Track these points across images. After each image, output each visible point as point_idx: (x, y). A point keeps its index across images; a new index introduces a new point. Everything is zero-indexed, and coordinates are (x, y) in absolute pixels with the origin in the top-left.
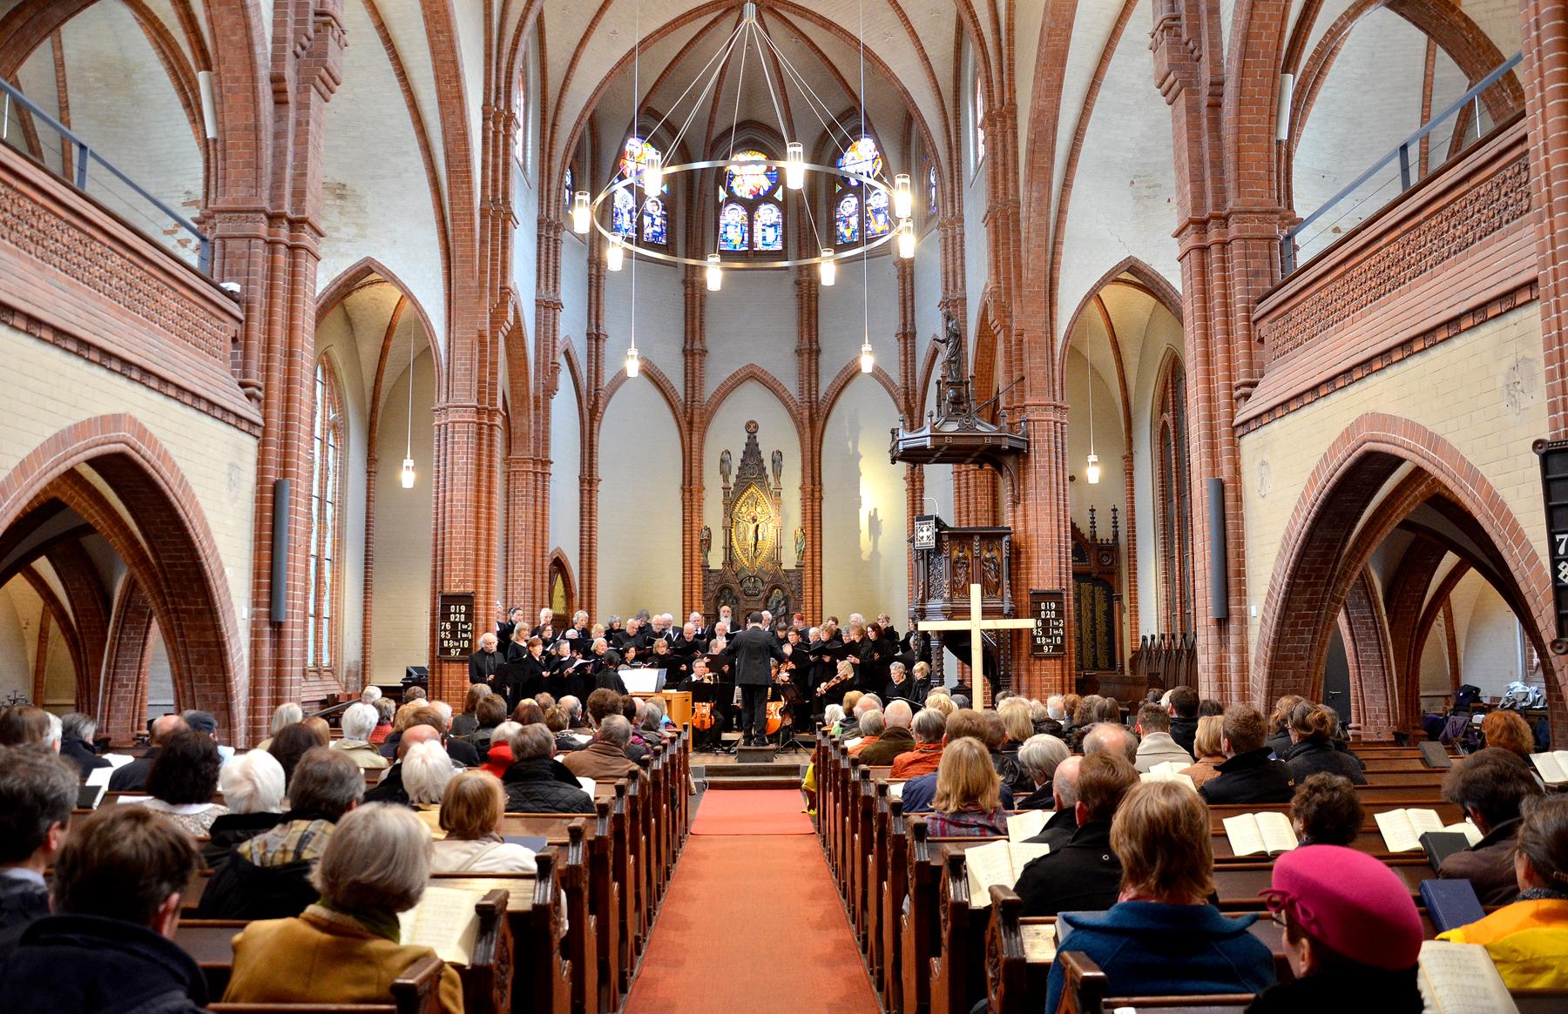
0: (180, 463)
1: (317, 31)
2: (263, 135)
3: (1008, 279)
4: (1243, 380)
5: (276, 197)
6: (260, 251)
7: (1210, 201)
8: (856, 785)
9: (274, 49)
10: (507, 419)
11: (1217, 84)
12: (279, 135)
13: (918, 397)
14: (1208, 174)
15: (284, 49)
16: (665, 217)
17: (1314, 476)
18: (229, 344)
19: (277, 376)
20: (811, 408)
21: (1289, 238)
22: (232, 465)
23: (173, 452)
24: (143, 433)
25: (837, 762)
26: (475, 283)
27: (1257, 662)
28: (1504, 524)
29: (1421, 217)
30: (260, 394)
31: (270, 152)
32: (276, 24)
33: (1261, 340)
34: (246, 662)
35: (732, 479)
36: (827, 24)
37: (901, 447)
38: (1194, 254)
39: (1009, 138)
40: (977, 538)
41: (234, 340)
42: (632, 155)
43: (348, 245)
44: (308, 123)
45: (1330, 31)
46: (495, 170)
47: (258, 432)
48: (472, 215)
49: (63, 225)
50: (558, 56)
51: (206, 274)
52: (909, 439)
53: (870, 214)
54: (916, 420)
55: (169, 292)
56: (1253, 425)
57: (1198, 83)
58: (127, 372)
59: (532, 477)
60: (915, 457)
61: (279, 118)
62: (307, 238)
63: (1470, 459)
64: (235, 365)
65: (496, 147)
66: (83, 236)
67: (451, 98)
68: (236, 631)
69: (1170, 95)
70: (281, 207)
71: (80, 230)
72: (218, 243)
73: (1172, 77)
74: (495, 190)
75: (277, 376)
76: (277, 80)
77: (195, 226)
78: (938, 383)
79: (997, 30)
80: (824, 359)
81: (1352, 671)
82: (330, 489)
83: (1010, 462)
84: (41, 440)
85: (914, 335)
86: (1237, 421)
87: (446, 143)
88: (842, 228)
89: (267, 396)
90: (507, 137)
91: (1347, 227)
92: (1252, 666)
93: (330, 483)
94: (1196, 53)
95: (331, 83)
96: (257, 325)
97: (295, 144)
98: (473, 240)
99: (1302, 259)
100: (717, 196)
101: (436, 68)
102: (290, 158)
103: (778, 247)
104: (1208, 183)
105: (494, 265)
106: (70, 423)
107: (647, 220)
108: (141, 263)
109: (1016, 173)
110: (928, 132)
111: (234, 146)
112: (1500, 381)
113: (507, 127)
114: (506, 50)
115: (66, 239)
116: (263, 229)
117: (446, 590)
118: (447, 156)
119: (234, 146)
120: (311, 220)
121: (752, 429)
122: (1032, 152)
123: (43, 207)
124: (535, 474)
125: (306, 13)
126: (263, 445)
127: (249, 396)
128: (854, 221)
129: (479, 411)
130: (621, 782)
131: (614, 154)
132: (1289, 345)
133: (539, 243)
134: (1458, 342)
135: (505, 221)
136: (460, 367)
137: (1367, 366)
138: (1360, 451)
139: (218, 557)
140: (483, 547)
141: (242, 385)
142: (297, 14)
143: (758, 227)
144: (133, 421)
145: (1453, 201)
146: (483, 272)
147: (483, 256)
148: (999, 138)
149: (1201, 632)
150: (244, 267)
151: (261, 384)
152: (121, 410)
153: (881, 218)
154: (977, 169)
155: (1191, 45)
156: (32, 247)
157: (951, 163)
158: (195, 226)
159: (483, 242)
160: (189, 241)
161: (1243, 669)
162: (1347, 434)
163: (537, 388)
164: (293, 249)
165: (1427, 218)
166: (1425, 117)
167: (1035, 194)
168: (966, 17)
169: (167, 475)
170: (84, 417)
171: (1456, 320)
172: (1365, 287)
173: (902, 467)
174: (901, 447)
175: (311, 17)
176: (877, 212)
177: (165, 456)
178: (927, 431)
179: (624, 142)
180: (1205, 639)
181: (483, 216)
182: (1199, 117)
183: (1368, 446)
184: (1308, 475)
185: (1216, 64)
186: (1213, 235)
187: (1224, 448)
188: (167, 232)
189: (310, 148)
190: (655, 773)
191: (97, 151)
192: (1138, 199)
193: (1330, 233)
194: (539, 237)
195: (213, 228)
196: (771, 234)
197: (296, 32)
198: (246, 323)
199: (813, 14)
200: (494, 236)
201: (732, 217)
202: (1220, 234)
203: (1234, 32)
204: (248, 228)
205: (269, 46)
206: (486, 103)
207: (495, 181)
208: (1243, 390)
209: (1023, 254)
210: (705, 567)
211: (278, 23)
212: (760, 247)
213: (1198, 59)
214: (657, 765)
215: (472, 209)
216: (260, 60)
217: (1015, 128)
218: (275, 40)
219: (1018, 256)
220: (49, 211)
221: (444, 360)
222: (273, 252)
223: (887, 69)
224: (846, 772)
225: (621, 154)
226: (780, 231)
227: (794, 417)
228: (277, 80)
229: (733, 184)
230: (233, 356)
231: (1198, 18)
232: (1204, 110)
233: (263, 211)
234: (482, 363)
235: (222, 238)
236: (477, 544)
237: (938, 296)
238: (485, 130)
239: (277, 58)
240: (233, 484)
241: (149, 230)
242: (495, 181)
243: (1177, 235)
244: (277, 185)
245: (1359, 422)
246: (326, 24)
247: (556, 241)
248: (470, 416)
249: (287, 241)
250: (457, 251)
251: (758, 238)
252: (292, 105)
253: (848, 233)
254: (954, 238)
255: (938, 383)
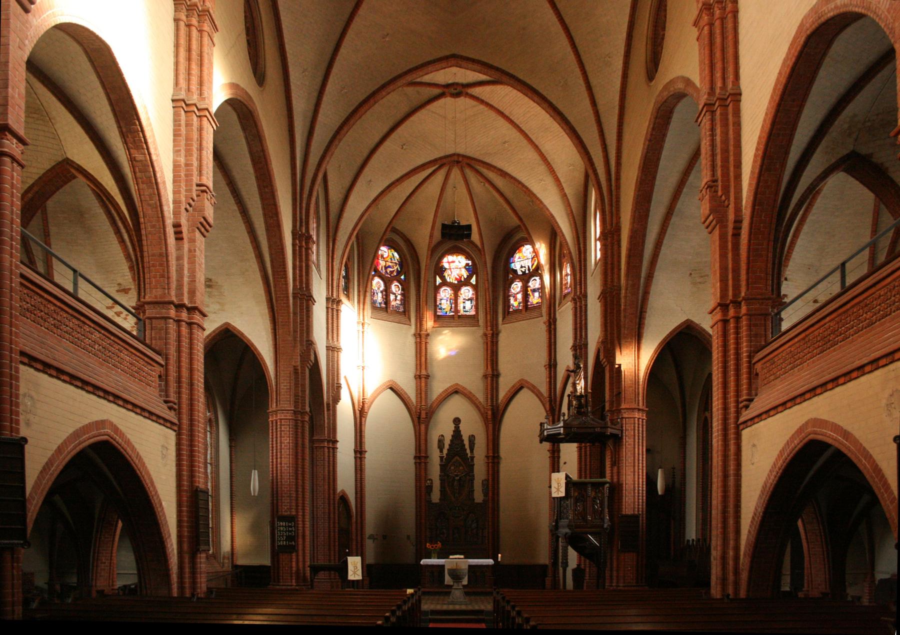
0: (137, 446)
1: (198, 196)
2: (170, 258)
3: (612, 334)
4: (745, 397)
5: (180, 294)
6: (172, 326)
7: (730, 293)
8: (514, 618)
9: (174, 208)
10: (311, 418)
11: (738, 221)
12: (179, 258)
13: (558, 403)
14: (730, 276)
15: (180, 207)
16: (401, 294)
17: (781, 452)
18: (158, 380)
19: (185, 397)
20: (492, 410)
21: (779, 313)
22: (163, 446)
23: (132, 439)
24: (116, 430)
25: (504, 607)
26: (290, 338)
27: (745, 554)
28: (880, 480)
29: (849, 306)
30: (176, 407)
31: (174, 268)
32: (174, 193)
33: (757, 374)
34: (175, 551)
35: (445, 451)
36: (504, 174)
37: (545, 433)
38: (719, 324)
39: (616, 247)
40: (589, 486)
41: (160, 376)
42: (382, 256)
43: (214, 315)
44: (195, 250)
45: (808, 188)
46: (301, 270)
47: (176, 428)
48: (288, 297)
49: (69, 317)
50: (335, 196)
51: (142, 339)
52: (550, 430)
53: (530, 292)
54: (556, 417)
55: (125, 351)
56: (749, 423)
57: (727, 221)
58: (107, 397)
59: (326, 450)
60: (554, 440)
61: (179, 249)
62: (197, 318)
63: (865, 445)
64: (161, 391)
65: (301, 256)
66: (29, 292)
67: (274, 226)
68: (170, 536)
69: (710, 228)
70: (182, 300)
71: (79, 319)
72: (147, 321)
73: (711, 218)
74: (301, 282)
75: (185, 397)
76: (177, 225)
77: (133, 311)
78: (569, 396)
79: (609, 180)
80: (501, 380)
81: (806, 559)
82: (209, 457)
83: (610, 444)
84: (67, 435)
85: (555, 365)
86: (741, 420)
87: (271, 255)
88: (512, 301)
89: (180, 408)
90: (307, 255)
91: (823, 299)
92: (742, 557)
93: (209, 452)
94: (726, 202)
95: (207, 227)
96: (172, 368)
97: (188, 263)
98: (289, 312)
99: (785, 326)
100: (435, 281)
101: (264, 209)
102: (186, 272)
103: (473, 313)
104: (730, 282)
105: (302, 327)
106: (81, 425)
107: (392, 297)
108: (109, 336)
109: (620, 269)
110: (565, 239)
111: (154, 266)
112: (884, 402)
113: (307, 243)
114: (305, 196)
115: (71, 325)
116: (326, 444)
117: (280, 513)
118: (272, 261)
119: (154, 266)
120: (200, 307)
121: (457, 421)
122: (629, 256)
123: (59, 307)
124: (329, 448)
125: (192, 185)
126: (179, 435)
127: (170, 408)
128: (519, 296)
129: (295, 412)
130: (394, 608)
131: (371, 256)
132: (772, 378)
133: (327, 312)
134: (863, 379)
135: (308, 301)
136: (284, 386)
137: (813, 391)
138: (806, 439)
139: (158, 496)
140: (300, 490)
141: (166, 402)
142: (186, 186)
143: (460, 300)
144: (111, 424)
145: (866, 298)
146: (295, 331)
147: (295, 322)
148: (609, 247)
149: (714, 539)
150: (163, 335)
151: (176, 401)
152: (105, 418)
153: (537, 294)
154: (596, 264)
155: (723, 197)
156: (55, 330)
157: (580, 261)
158: (133, 311)
159: (295, 314)
160: (121, 313)
161: (737, 557)
162: (800, 430)
163: (328, 398)
164: (190, 324)
165: (853, 307)
166: (874, 231)
167: (630, 282)
168: (590, 172)
169: (130, 452)
170: (86, 422)
171: (862, 367)
172: (816, 346)
173: (547, 445)
174: (545, 433)
175: (195, 188)
176: (534, 291)
177: (128, 442)
178: (561, 424)
179: (378, 249)
180: (716, 542)
181: (294, 298)
182: (727, 242)
183: (812, 437)
184: (777, 452)
185: (738, 209)
186: (732, 312)
187: (732, 436)
188: (108, 308)
189: (197, 265)
190: (404, 612)
191: (82, 272)
192: (694, 284)
193: (811, 303)
194: (327, 308)
195: (144, 312)
196: (468, 305)
197: (186, 197)
198: (166, 367)
199: (495, 167)
200: (301, 310)
201: (445, 294)
202: (736, 312)
203: (749, 191)
204: (163, 312)
205: (171, 206)
206: (294, 226)
207: (301, 276)
208: (744, 403)
209: (622, 319)
210: (429, 502)
211: (176, 192)
212: (462, 313)
213: (728, 206)
214: (405, 608)
215: (287, 294)
216: (166, 214)
217: (619, 241)
218: (175, 202)
219: (619, 321)
220: (62, 309)
221: (274, 384)
222: (179, 326)
223: (541, 202)
224: (509, 612)
225: (376, 256)
226: (474, 303)
227: (482, 414)
228: (177, 225)
229: (446, 274)
230: (160, 385)
231: (728, 180)
232: (730, 238)
233: (172, 303)
234: (296, 385)
235: (150, 318)
236: (297, 488)
237: (570, 342)
238: (294, 245)
239: (176, 213)
240: (164, 456)
241: (98, 307)
242: (301, 276)
243: (711, 313)
244: (180, 287)
245: (807, 423)
246: (203, 191)
247: (337, 311)
248: (289, 416)
249: (186, 319)
250: (280, 319)
251: (461, 307)
252: (186, 240)
253: (516, 304)
254: (581, 307)
255: (569, 396)
